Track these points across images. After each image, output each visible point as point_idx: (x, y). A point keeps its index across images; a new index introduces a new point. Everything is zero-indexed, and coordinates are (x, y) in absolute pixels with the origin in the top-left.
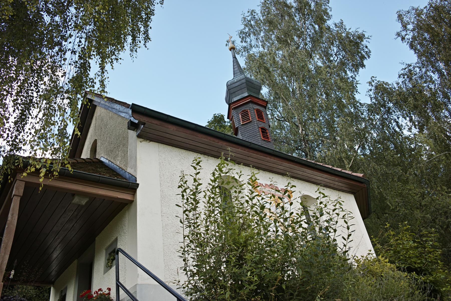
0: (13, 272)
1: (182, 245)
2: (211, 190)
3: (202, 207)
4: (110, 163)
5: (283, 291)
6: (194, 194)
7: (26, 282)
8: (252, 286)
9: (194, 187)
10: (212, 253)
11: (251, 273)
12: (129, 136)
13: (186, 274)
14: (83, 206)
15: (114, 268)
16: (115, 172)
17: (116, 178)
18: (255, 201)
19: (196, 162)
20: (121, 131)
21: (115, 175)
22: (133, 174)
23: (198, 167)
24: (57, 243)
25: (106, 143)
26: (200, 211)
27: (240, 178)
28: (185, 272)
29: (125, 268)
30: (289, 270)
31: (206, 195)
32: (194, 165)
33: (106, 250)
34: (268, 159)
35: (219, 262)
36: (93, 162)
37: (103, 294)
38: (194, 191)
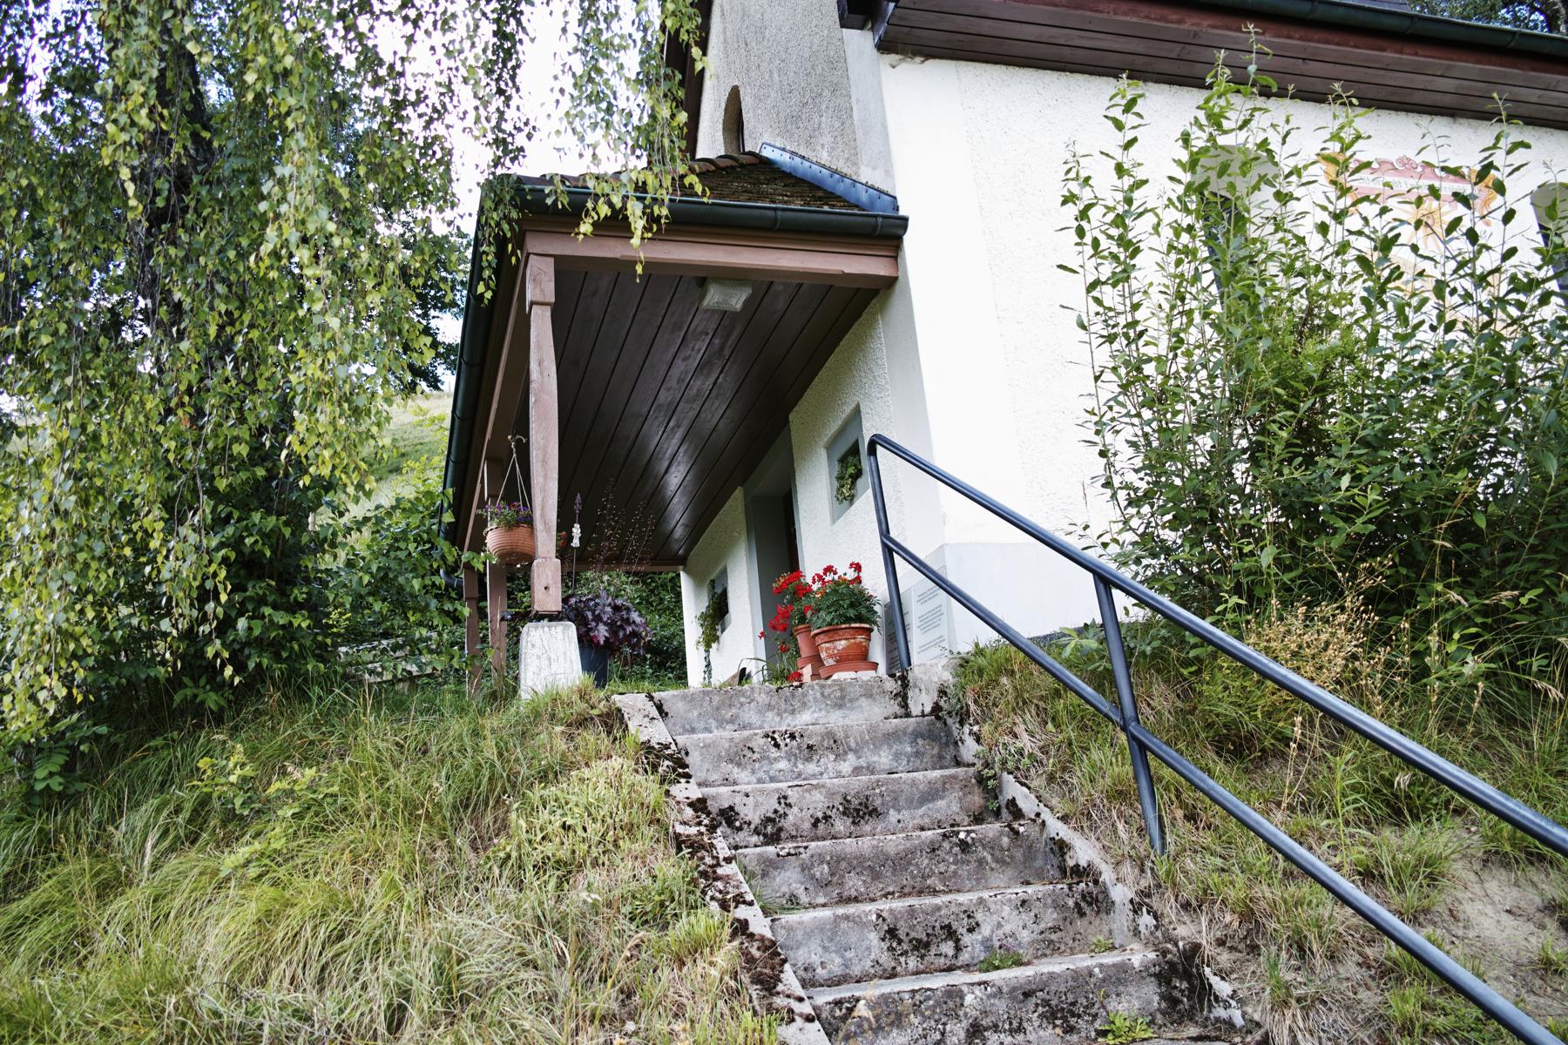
0: (576, 531)
1: (1091, 404)
2: (1179, 198)
3: (1151, 269)
4: (798, 160)
5: (1477, 535)
6: (1119, 221)
7: (613, 561)
8: (1359, 521)
9: (1120, 196)
10: (1200, 427)
11: (1353, 479)
12: (849, 54)
13: (1114, 496)
14: (735, 316)
15: (865, 500)
16: (819, 188)
17: (826, 208)
18: (1353, 222)
19: (1124, 102)
20: (816, 42)
21: (820, 199)
22: (883, 187)
23: (1129, 120)
24: (675, 442)
25: (773, 94)
26: (1147, 282)
27: (1284, 142)
28: (1109, 492)
29: (898, 499)
30: (1496, 465)
31: (1159, 224)
32: (1117, 113)
33: (830, 448)
34: (1390, 56)
35: (1222, 454)
36: (742, 166)
37: (842, 582)
38: (1120, 210)
